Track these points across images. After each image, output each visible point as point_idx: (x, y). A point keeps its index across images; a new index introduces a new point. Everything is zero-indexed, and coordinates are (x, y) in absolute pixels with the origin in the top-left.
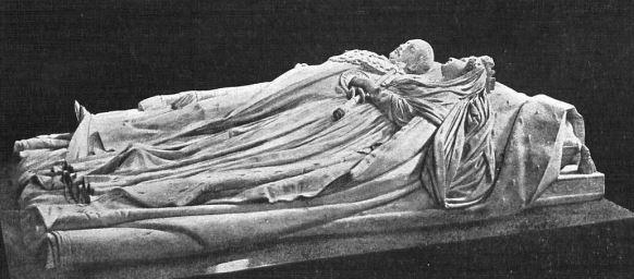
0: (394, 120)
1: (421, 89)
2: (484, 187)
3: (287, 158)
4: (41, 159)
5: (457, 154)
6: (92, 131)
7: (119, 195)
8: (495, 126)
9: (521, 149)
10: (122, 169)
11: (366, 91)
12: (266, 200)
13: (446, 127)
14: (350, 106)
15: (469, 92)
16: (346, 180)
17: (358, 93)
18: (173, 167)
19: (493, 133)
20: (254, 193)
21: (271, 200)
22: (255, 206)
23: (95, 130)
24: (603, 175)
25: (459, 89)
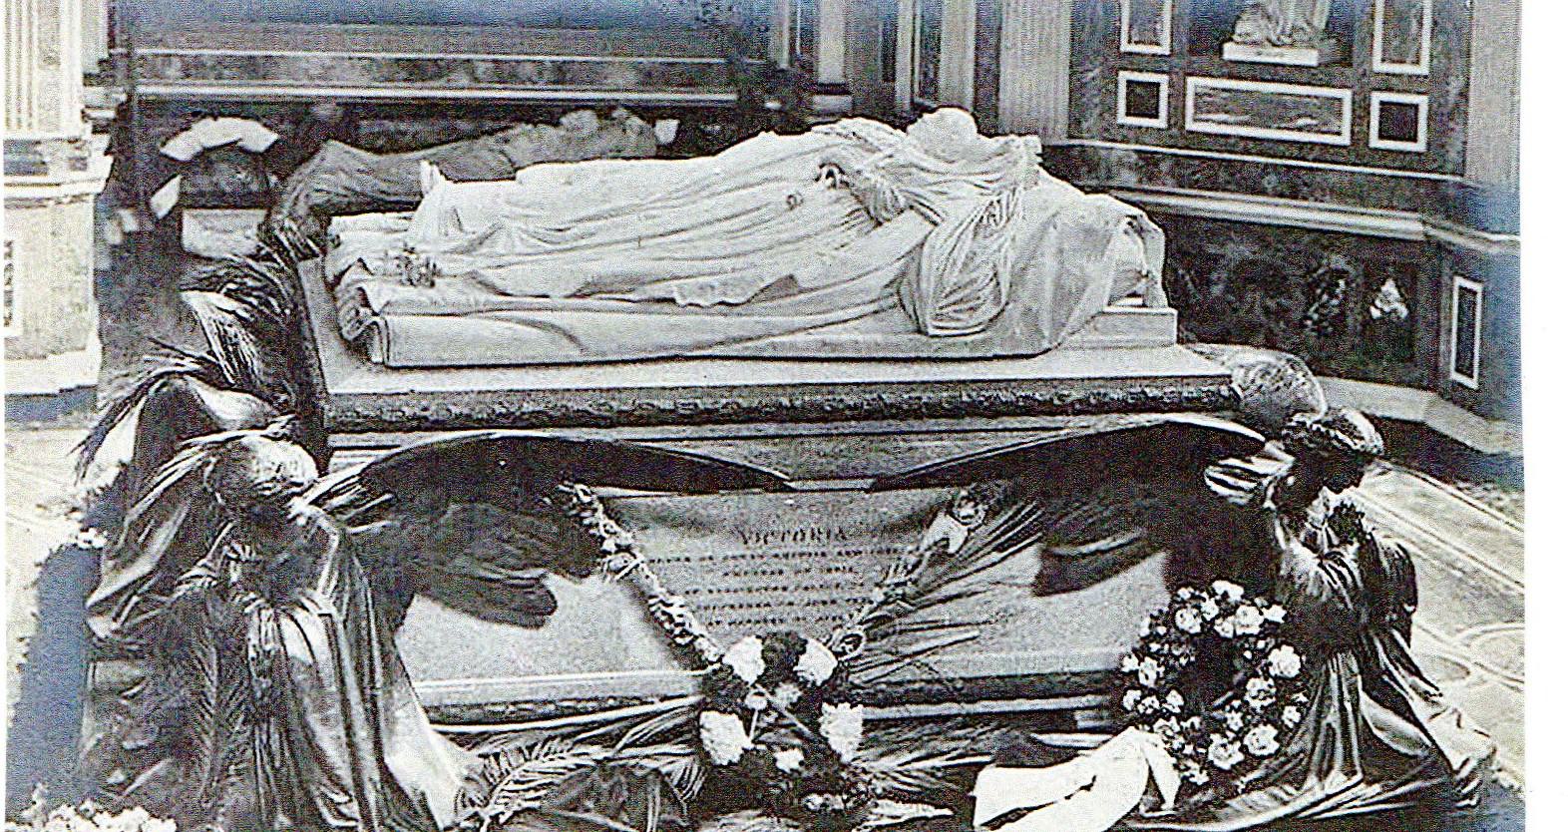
0: (872, 214)
1: (923, 174)
2: (989, 310)
3: (346, 444)
4: (1449, 508)
5: (954, 263)
6: (448, 206)
7: (475, 279)
8: (1020, 229)
9: (1049, 263)
10: (484, 250)
11: (842, 172)
12: (672, 301)
13: (945, 228)
14: (819, 193)
15: (995, 185)
16: (788, 284)
17: (830, 174)
18: (549, 252)
19: (1013, 240)
20: (658, 290)
21: (679, 301)
22: (245, 99)
23: (454, 202)
24: (1175, 312)
25: (979, 179)
